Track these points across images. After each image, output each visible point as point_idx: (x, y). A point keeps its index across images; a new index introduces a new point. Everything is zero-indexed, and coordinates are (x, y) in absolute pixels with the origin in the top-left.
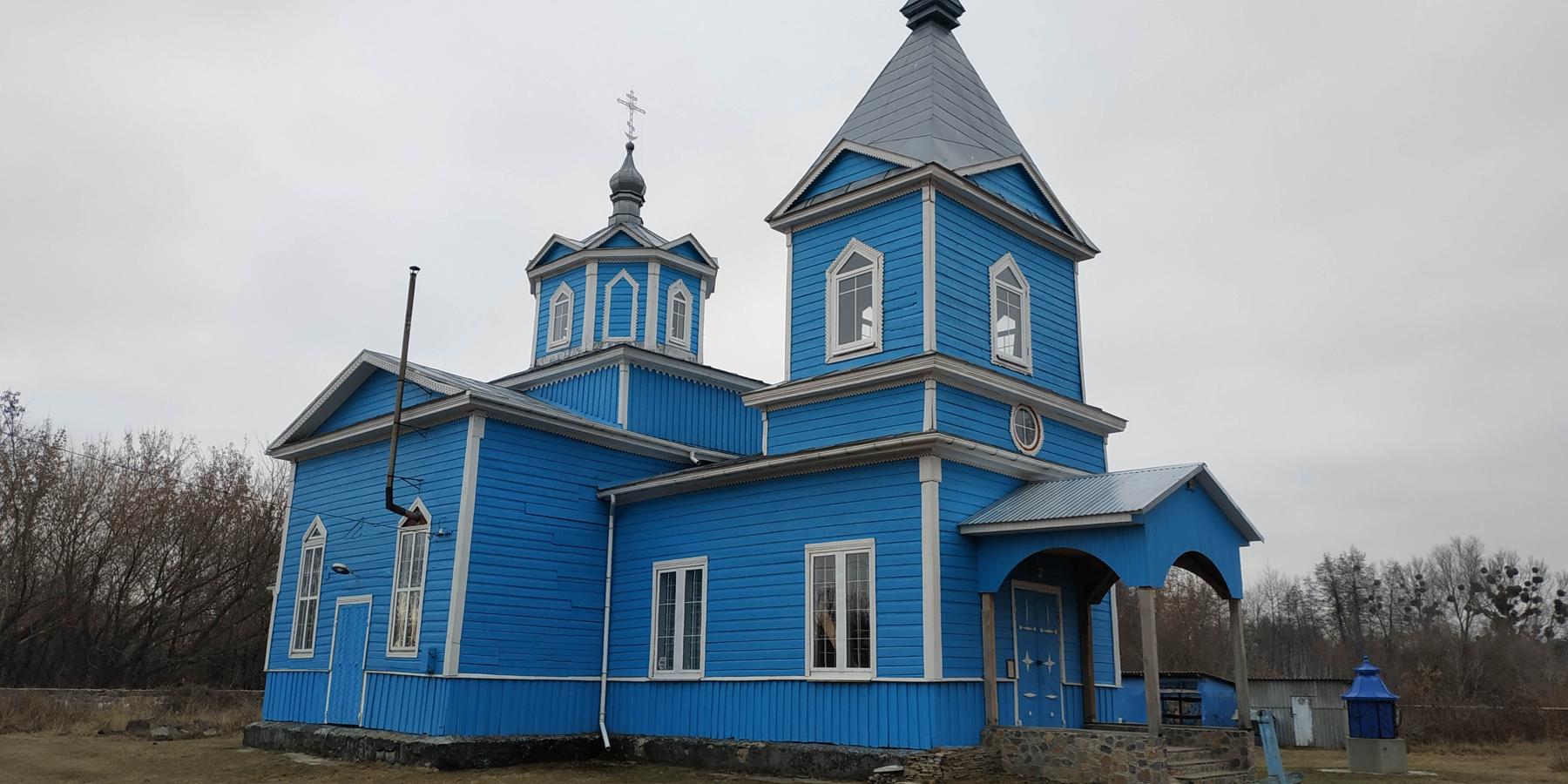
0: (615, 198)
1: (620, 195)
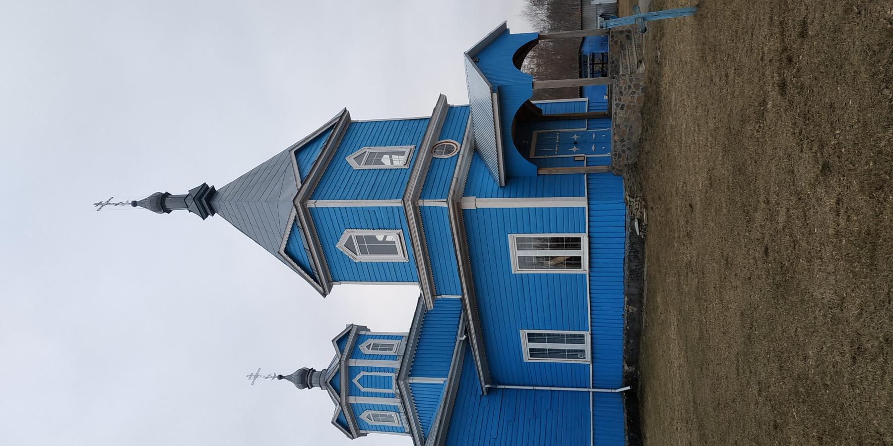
0: (310, 386)
1: (308, 383)
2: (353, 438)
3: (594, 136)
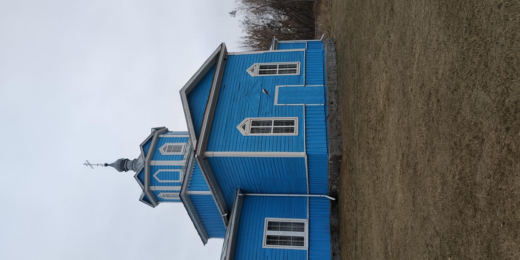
0: (126, 170)
1: (125, 168)
2: (154, 207)
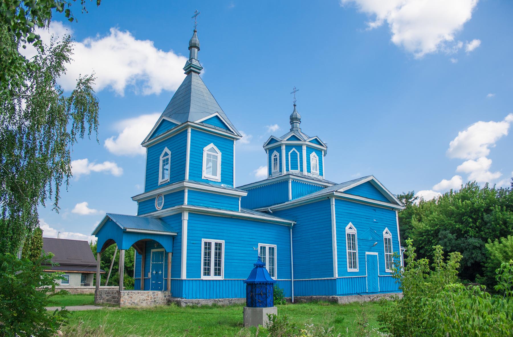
3: (159, 283)
